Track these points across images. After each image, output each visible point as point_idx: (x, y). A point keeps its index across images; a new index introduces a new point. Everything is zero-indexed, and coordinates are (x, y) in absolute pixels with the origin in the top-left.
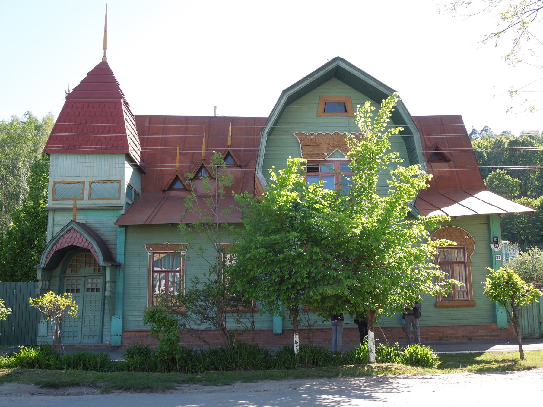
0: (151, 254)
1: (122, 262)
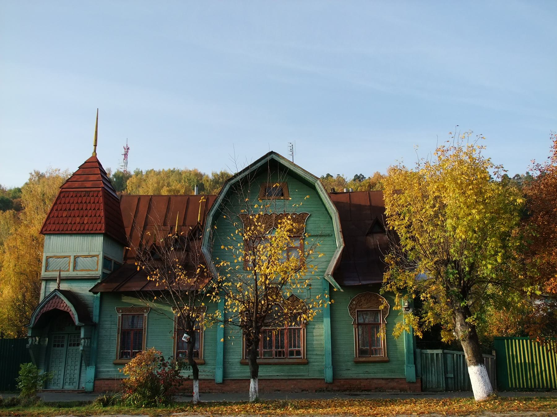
0: (120, 315)
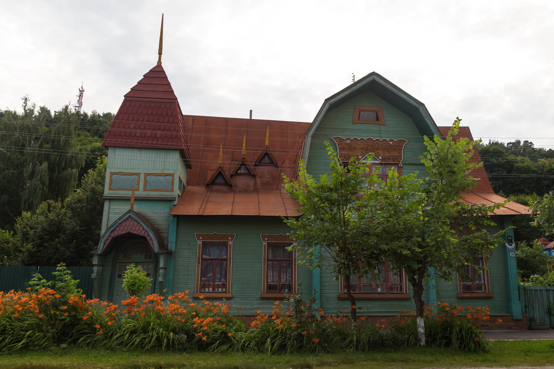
0: (200, 243)
1: (173, 249)
